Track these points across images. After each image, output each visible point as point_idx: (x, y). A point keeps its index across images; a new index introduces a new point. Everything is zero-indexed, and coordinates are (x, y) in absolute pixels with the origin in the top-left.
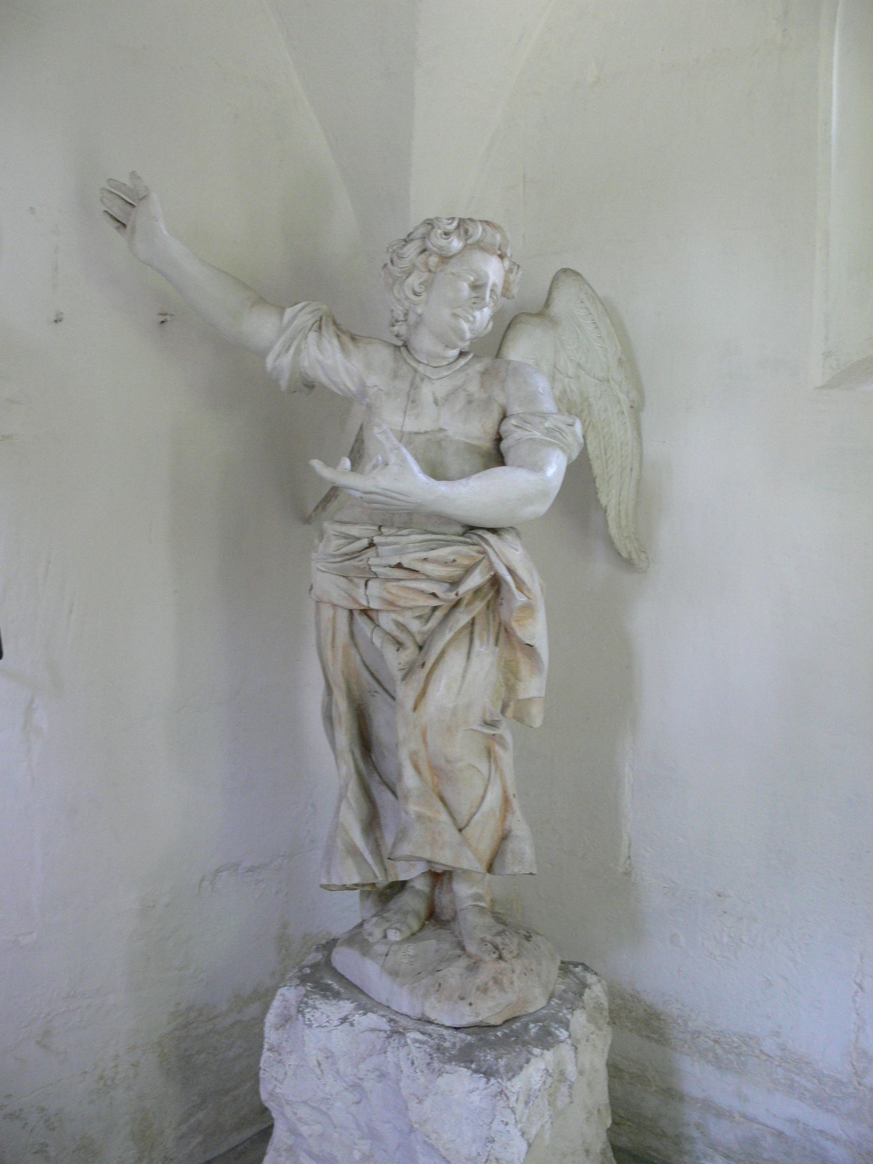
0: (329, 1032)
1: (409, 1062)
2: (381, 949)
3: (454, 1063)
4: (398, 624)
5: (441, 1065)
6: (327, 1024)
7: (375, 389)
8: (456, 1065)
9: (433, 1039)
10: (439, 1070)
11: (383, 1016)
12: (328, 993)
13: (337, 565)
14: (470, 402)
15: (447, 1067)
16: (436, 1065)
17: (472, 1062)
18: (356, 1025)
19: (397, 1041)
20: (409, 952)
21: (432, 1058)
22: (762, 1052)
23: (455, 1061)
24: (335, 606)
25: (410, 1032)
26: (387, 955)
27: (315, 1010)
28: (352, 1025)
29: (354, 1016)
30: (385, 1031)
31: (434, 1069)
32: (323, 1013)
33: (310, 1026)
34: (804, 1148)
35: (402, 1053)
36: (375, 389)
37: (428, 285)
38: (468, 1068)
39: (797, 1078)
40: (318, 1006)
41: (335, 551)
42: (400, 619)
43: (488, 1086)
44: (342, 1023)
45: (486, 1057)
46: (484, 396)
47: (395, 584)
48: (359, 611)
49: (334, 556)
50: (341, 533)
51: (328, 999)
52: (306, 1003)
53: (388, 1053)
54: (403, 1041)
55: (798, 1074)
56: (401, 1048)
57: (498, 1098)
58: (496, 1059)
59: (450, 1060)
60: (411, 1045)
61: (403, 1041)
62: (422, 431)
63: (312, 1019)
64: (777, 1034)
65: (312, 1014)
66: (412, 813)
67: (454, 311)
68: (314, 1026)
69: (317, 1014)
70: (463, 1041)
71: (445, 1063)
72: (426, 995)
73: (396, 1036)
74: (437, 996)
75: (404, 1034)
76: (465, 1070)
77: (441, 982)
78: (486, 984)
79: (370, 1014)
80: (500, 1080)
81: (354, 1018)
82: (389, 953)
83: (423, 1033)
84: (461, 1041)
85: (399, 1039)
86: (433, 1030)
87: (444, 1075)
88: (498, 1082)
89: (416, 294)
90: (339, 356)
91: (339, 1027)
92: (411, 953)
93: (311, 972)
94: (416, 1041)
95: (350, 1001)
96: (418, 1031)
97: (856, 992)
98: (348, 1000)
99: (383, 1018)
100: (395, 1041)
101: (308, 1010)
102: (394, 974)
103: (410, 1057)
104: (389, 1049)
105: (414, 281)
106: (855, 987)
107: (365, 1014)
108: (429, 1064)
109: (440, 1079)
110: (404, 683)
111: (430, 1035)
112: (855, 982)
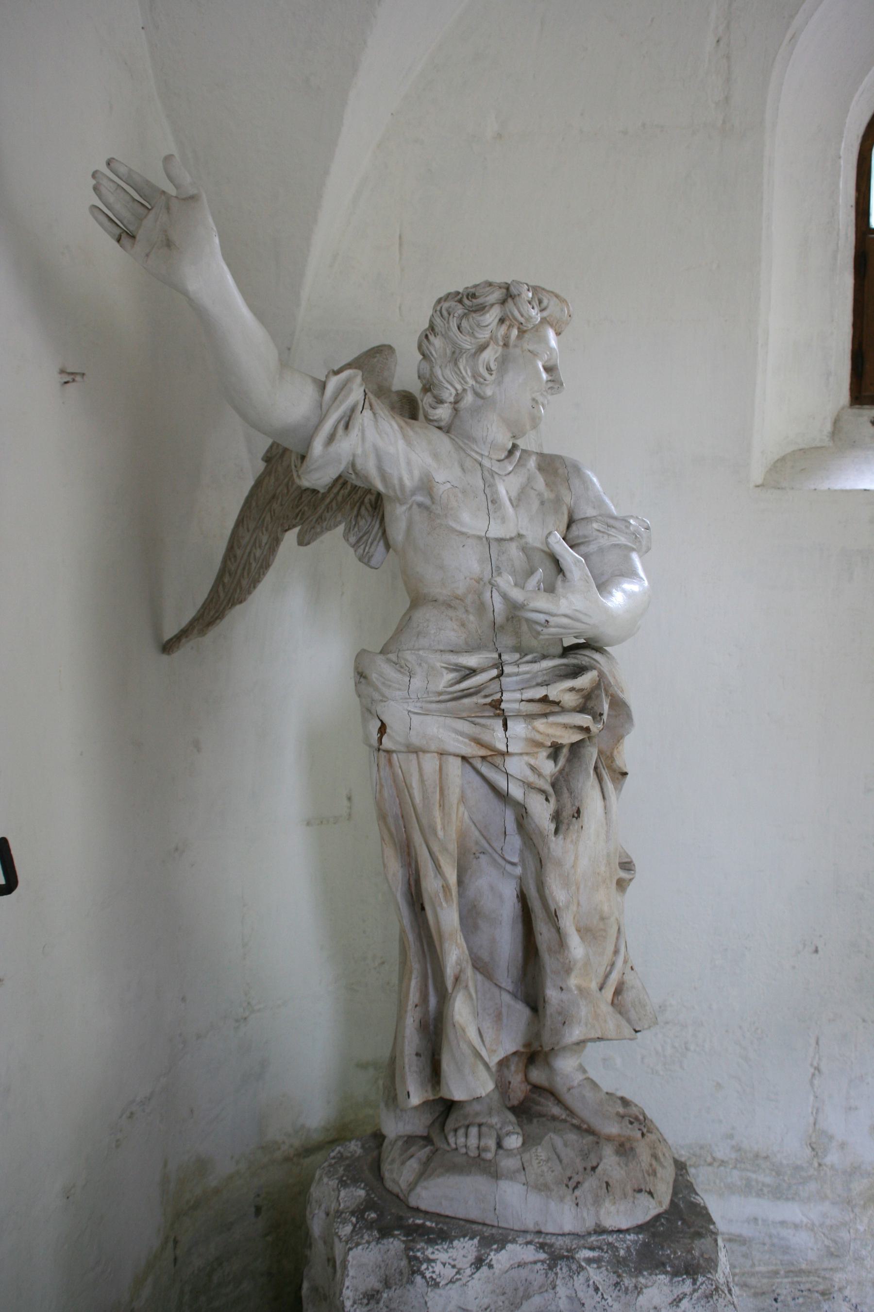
0: (465, 1285)
1: (591, 1291)
2: (509, 1163)
3: (645, 1273)
4: (533, 768)
5: (634, 1280)
6: (458, 1276)
7: (448, 485)
8: (650, 1274)
9: (607, 1252)
10: (636, 1287)
11: (528, 1243)
12: (431, 1236)
13: (443, 706)
14: (542, 503)
15: (642, 1280)
16: (628, 1282)
17: (664, 1265)
18: (495, 1266)
19: (565, 1269)
20: (541, 1156)
21: (619, 1276)
22: (714, 1159)
23: (645, 1270)
24: (442, 754)
25: (578, 1252)
26: (524, 1169)
27: (433, 1264)
28: (490, 1266)
29: (489, 1255)
30: (543, 1262)
31: (627, 1289)
32: (444, 1264)
33: (437, 1285)
34: (764, 1244)
35: (579, 1280)
36: (448, 485)
37: (504, 362)
38: (666, 1273)
39: (754, 1176)
40: (432, 1257)
41: (452, 685)
42: (532, 761)
43: (696, 1287)
44: (478, 1269)
45: (675, 1253)
46: (552, 496)
47: (544, 720)
48: (480, 759)
49: (440, 694)
50: (456, 665)
51: (437, 1244)
52: (416, 1258)
53: (558, 1289)
54: (574, 1267)
55: (754, 1172)
56: (575, 1277)
57: (715, 1297)
58: (689, 1251)
59: (639, 1272)
60: (588, 1267)
61: (574, 1267)
62: (508, 537)
63: (434, 1276)
64: (731, 1137)
65: (431, 1269)
66: (574, 988)
67: (534, 395)
68: (441, 1285)
69: (438, 1268)
70: (635, 1242)
71: (637, 1277)
72: (597, 1202)
73: (563, 1264)
74: (611, 1197)
75: (573, 1258)
76: (663, 1276)
77: (606, 1179)
78: (651, 1165)
79: (509, 1246)
80: (709, 1276)
81: (490, 1258)
82: (525, 1166)
83: (592, 1249)
84: (634, 1244)
85: (567, 1265)
86: (597, 1241)
87: (644, 1290)
88: (709, 1278)
89: (489, 369)
90: (401, 444)
91: (476, 1276)
92: (543, 1158)
93: (378, 1215)
94: (589, 1261)
95: (467, 1238)
96: (585, 1248)
97: (813, 1075)
98: (464, 1236)
99: (529, 1246)
100: (562, 1269)
101: (424, 1266)
102: (542, 1188)
103: (591, 1282)
104: (558, 1282)
105: (490, 355)
106: (812, 1070)
107: (503, 1247)
108: (617, 1284)
109: (641, 1298)
110: (561, 837)
111: (600, 1248)
112: (812, 1065)
